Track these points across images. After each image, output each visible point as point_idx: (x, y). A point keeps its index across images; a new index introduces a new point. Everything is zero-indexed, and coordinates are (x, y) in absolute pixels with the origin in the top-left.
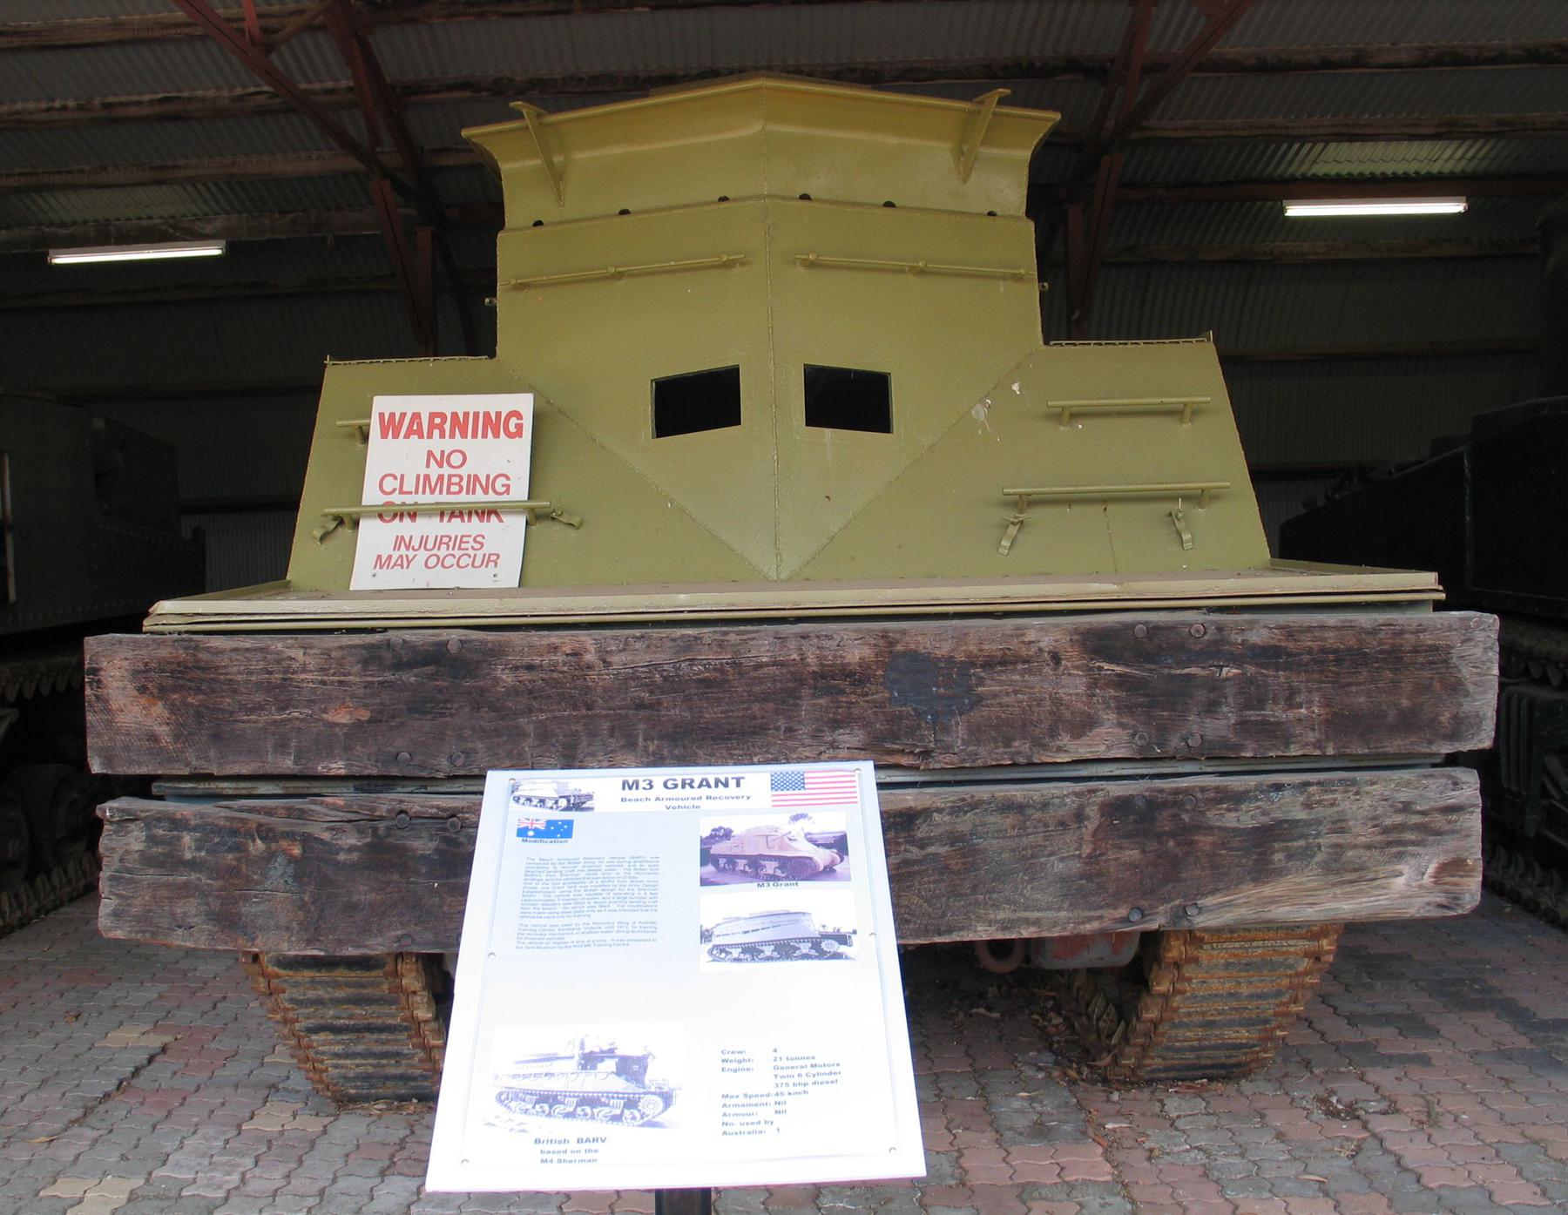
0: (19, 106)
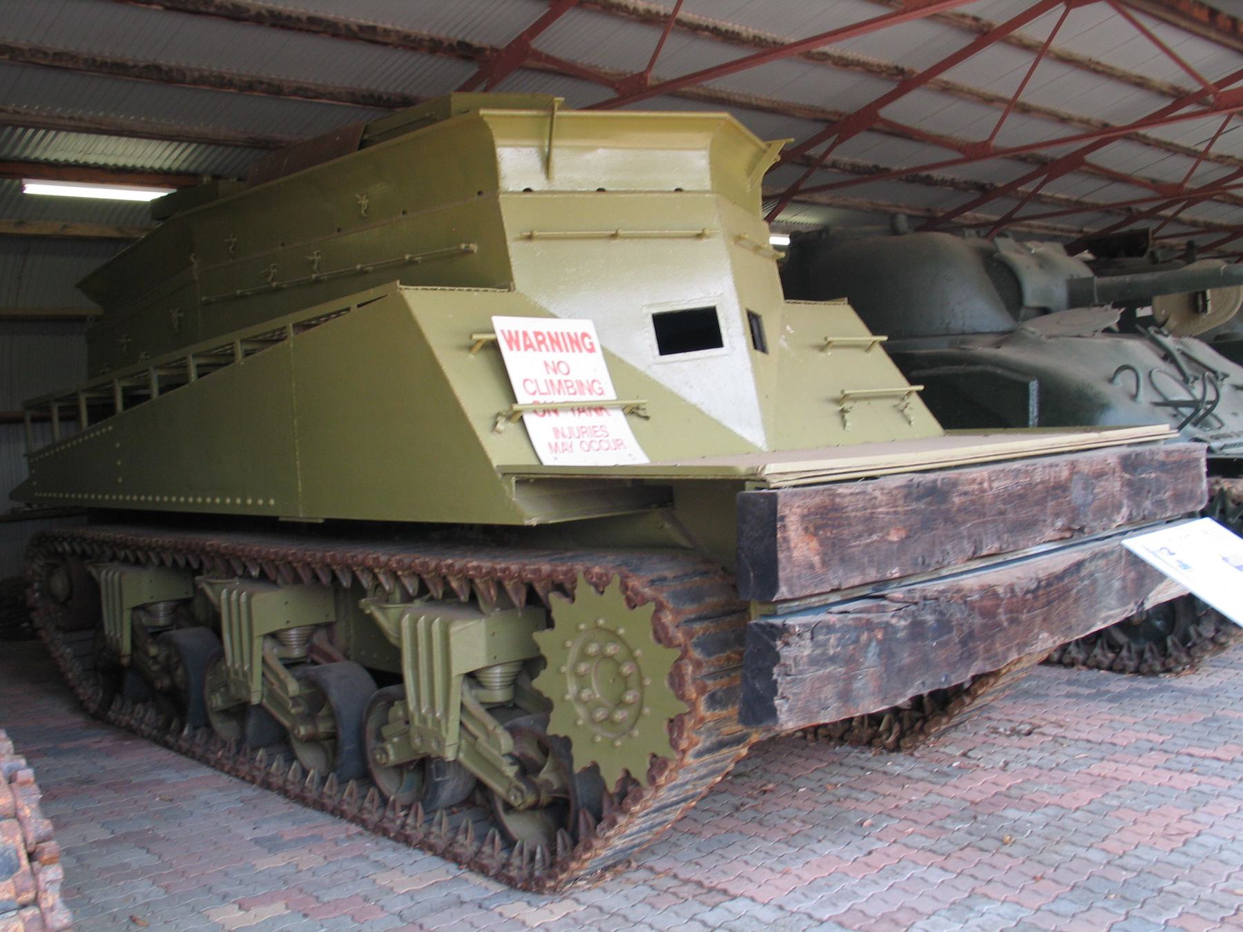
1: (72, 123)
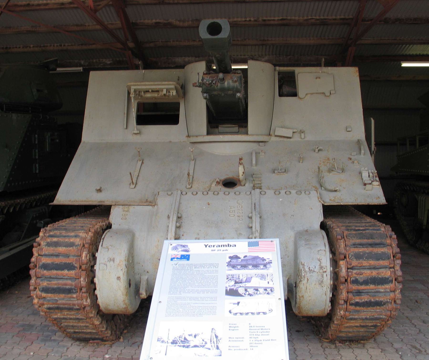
0: (235, 20)
1: (419, 41)
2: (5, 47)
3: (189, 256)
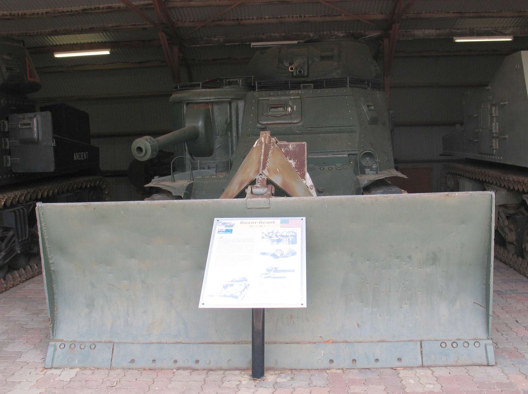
2: (235, 18)
3: (232, 230)
